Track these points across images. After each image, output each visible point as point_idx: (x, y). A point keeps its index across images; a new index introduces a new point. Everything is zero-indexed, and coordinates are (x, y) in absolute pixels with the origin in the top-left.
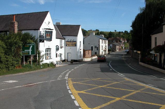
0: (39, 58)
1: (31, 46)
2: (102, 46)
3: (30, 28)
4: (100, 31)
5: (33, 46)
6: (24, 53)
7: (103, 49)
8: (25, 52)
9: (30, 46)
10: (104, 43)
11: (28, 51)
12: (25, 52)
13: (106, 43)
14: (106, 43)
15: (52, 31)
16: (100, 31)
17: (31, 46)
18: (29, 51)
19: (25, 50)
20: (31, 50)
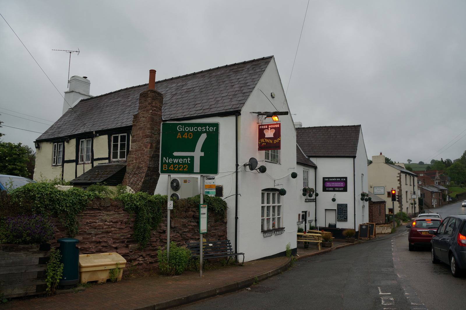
0: (159, 128)
1: (203, 137)
2: (407, 192)
3: (212, 110)
4: (311, 188)
5: (208, 133)
6: (169, 164)
7: (410, 202)
8: (176, 161)
9: (197, 135)
10: (411, 185)
11: (187, 157)
12: (176, 161)
13: (414, 186)
14: (414, 186)
15: (262, 217)
16: (311, 188)
17: (203, 137)
18: (192, 158)
19: (176, 154)
20: (202, 154)
